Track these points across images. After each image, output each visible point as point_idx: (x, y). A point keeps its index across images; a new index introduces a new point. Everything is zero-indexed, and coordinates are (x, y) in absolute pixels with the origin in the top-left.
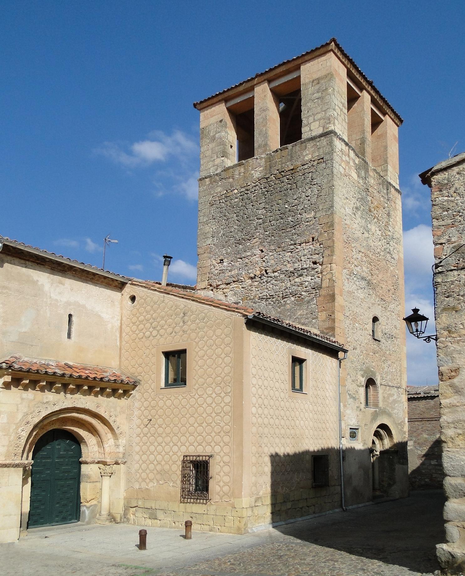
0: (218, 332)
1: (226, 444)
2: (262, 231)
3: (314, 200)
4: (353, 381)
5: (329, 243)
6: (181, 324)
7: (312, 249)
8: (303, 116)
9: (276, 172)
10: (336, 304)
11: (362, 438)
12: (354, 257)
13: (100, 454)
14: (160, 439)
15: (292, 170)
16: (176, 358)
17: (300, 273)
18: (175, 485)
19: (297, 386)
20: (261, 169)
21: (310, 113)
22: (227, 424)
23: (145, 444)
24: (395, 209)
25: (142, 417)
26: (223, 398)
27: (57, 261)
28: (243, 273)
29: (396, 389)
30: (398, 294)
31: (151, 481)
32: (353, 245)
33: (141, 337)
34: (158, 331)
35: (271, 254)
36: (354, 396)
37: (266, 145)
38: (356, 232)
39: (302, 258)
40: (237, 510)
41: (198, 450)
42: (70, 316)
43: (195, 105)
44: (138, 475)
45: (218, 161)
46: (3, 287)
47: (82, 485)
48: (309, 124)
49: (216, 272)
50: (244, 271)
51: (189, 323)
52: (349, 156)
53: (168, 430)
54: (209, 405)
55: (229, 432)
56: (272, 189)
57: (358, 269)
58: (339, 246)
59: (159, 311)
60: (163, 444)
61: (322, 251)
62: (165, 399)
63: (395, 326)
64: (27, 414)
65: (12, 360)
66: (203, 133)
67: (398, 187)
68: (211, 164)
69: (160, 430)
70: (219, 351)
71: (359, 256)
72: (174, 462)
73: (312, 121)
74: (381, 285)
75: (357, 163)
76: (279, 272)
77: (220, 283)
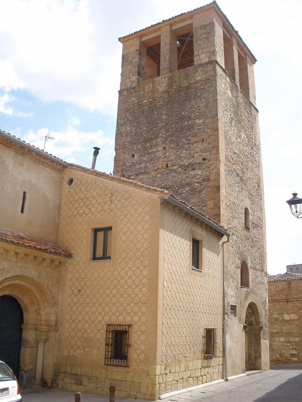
1: (143, 314)
6: (109, 203)
20: (165, 85)
22: (144, 295)
33: (75, 215)
42: (25, 193)
44: (68, 342)
47: (22, 349)
48: (199, 55)
49: (129, 164)
51: (116, 202)
54: (130, 277)
62: (93, 271)
70: (139, 227)
72: (98, 330)
77: (131, 174)
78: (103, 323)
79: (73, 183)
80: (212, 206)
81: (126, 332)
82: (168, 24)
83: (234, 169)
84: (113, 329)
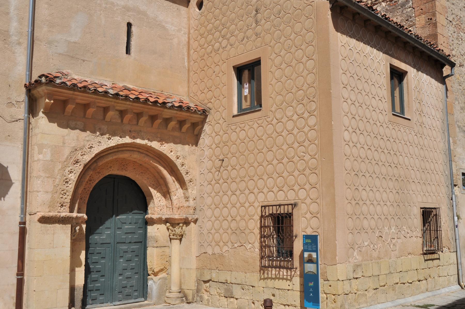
0: (298, 27)
6: (254, 25)
13: (168, 209)
16: (248, 71)
18: (253, 249)
19: (398, 109)
23: (217, 194)
26: (306, 120)
31: (225, 244)
33: (209, 51)
40: (330, 283)
41: (278, 198)
42: (129, 25)
51: (263, 21)
53: (242, 172)
55: (315, 168)
60: (238, 193)
64: (76, 150)
65: (55, 74)
69: (234, 174)
78: (256, 204)
79: (203, 6)
80: (423, 22)
81: (289, 216)
84: (271, 212)
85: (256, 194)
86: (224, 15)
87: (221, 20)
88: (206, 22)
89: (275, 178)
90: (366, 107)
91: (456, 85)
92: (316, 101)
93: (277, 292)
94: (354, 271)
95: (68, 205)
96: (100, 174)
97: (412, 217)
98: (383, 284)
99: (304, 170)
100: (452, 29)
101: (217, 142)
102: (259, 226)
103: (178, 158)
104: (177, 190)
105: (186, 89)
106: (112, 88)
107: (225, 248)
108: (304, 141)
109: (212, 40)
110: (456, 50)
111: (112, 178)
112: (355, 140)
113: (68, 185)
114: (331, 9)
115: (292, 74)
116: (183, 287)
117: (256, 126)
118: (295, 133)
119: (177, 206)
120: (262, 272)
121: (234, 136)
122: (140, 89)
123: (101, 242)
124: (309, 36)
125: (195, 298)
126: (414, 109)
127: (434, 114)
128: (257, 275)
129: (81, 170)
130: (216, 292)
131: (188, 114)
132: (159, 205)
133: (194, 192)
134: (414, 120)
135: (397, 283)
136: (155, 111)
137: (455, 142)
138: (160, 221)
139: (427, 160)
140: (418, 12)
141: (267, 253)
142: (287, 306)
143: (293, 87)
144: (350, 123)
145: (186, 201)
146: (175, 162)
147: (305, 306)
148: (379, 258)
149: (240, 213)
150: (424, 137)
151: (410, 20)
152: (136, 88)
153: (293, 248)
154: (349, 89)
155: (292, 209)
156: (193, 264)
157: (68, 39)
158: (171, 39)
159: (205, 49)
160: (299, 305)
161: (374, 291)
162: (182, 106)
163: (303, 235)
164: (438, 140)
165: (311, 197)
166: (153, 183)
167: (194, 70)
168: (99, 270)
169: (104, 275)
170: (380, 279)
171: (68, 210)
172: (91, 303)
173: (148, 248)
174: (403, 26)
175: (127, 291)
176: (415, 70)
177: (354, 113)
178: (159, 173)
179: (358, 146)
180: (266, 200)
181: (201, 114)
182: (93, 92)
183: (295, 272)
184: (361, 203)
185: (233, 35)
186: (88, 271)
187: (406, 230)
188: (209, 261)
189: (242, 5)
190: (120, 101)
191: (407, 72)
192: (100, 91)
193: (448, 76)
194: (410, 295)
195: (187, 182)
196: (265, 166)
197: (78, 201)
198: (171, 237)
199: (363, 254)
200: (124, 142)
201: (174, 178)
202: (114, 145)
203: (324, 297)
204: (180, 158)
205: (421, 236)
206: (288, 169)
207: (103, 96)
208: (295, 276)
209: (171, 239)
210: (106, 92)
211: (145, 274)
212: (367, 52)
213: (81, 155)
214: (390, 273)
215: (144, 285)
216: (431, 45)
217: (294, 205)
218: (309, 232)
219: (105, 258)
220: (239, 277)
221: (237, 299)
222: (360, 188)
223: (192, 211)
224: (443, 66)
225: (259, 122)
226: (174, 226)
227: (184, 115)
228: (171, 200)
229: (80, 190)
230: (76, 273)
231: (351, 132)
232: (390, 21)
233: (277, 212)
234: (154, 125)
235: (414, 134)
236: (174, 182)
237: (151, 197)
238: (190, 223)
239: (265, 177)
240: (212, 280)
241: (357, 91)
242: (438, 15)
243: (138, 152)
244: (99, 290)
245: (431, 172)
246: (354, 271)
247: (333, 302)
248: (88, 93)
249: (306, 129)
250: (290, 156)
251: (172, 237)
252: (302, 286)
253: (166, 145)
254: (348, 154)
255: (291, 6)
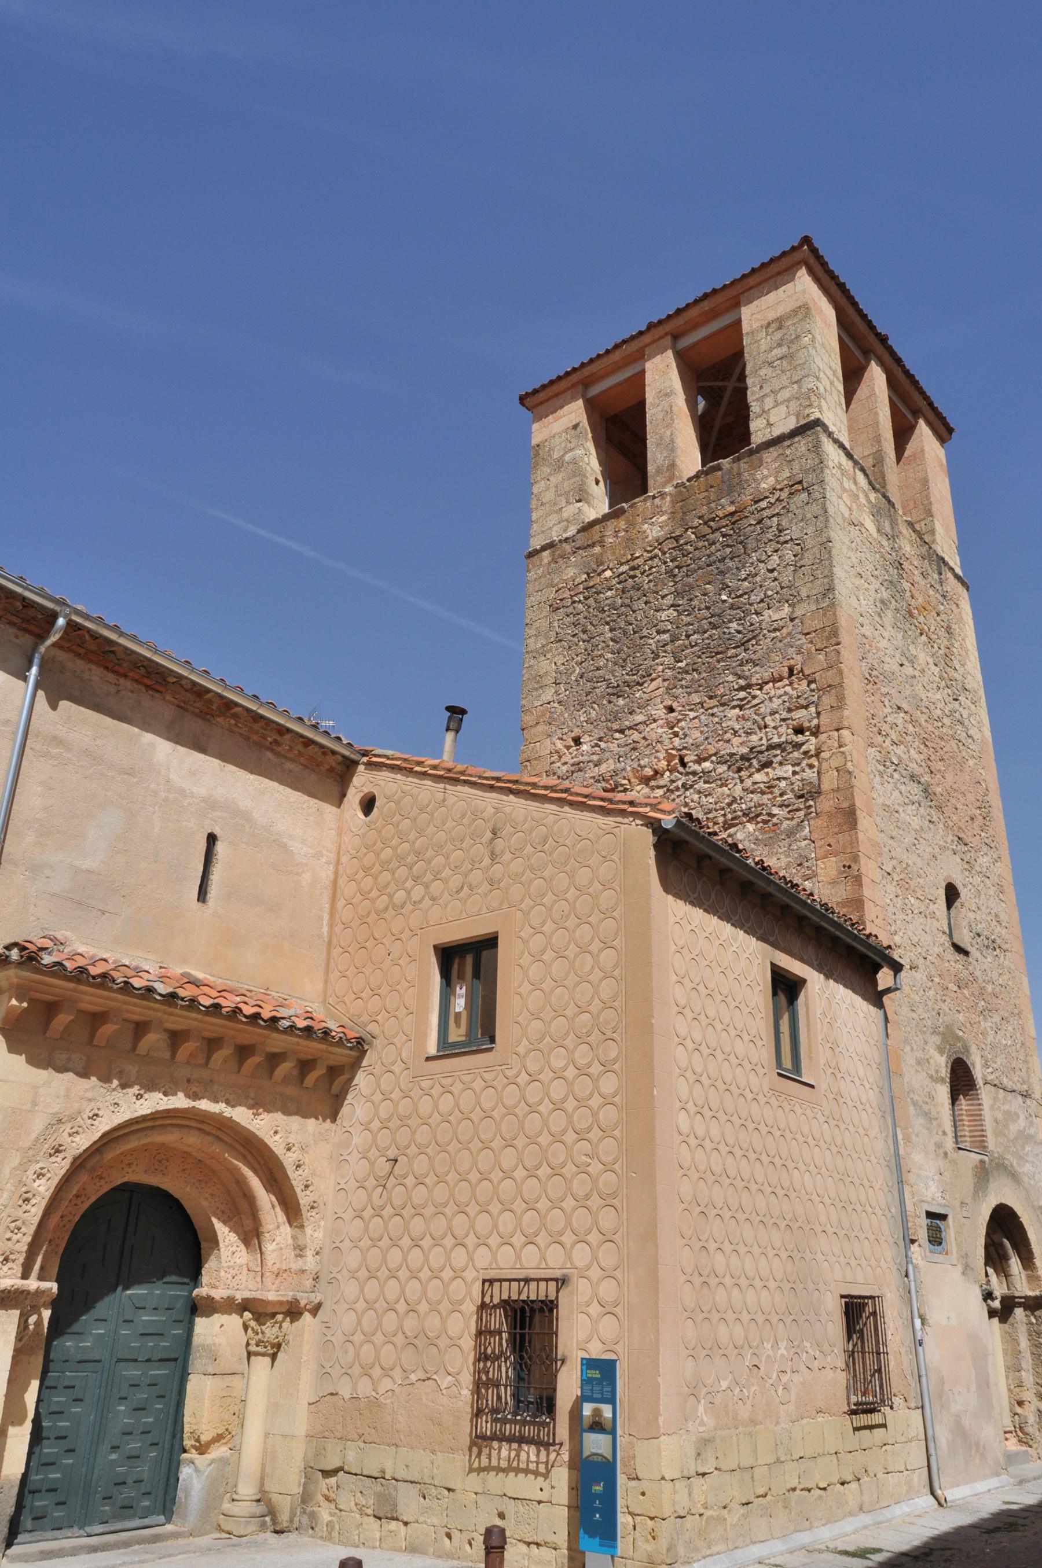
0: (583, 875)
2: (669, 660)
3: (787, 576)
4: (919, 1063)
5: (830, 677)
6: (487, 861)
7: (791, 697)
8: (751, 397)
9: (696, 522)
10: (861, 835)
11: (959, 1247)
12: (889, 719)
14: (418, 1225)
15: (732, 514)
16: (469, 961)
17: (763, 758)
18: (454, 1389)
19: (787, 1063)
20: (664, 518)
21: (767, 389)
22: (608, 1168)
24: (960, 620)
25: (373, 1153)
26: (595, 1080)
27: (194, 684)
28: (629, 769)
29: (1020, 1098)
30: (991, 832)
31: (387, 1372)
32: (884, 690)
33: (382, 907)
34: (427, 886)
35: (692, 714)
36: (926, 1108)
37: (673, 466)
38: (887, 659)
39: (768, 719)
40: (644, 1485)
41: (524, 1259)
42: (212, 839)
43: (522, 399)
44: (351, 1350)
45: (569, 511)
46: (54, 738)
49: (565, 768)
50: (629, 762)
51: (507, 856)
52: (855, 483)
53: (441, 1193)
55: (614, 1195)
56: (689, 562)
57: (900, 750)
58: (853, 685)
59: (432, 829)
61: (815, 699)
62: (436, 1091)
63: (996, 916)
64: (60, 1121)
65: (42, 943)
66: (537, 455)
67: (959, 571)
68: (553, 519)
69: (420, 1194)
71: (900, 718)
73: (771, 405)
74: (953, 801)
75: (873, 501)
76: (714, 758)
78: (470, 1274)
79: (375, 809)
80: (834, 872)
81: (549, 1307)
82: (666, 334)
83: (899, 758)
84: (505, 1297)
85: (471, 1248)
86: (421, 833)
87: (414, 843)
88: (379, 842)
89: (519, 1212)
90: (724, 1056)
91: (905, 1011)
92: (618, 1039)
93: (510, 1508)
94: (699, 1454)
95: (22, 1260)
96: (103, 1182)
97: (824, 1318)
98: (761, 1491)
99: (587, 1197)
100: (891, 888)
101: (383, 1115)
102: (473, 1331)
103: (289, 1149)
104: (278, 1227)
105: (320, 987)
106: (162, 979)
107: (386, 1384)
108: (589, 1129)
109: (388, 884)
110: (901, 934)
111: (129, 1191)
112: (700, 1132)
113: (29, 1207)
114: (656, 846)
115: (567, 975)
116: (270, 1486)
117: (478, 1084)
118: (570, 1110)
119: (275, 1269)
120: (475, 1450)
121: (425, 1105)
122: (220, 983)
123: (79, 1357)
124: (607, 898)
125: (296, 1519)
126: (822, 1062)
127: (861, 1074)
128: (461, 1460)
129: (63, 1171)
130: (353, 1503)
131: (324, 1047)
132: (232, 1264)
133: (319, 1235)
134: (822, 1086)
135: (794, 1489)
136: (249, 1035)
137: (907, 1139)
138: (231, 1306)
139: (850, 1179)
140: (823, 850)
141: (490, 1402)
142: (534, 1547)
143: (567, 1005)
144: (691, 1093)
145: (297, 1256)
146: (281, 1158)
147: (582, 1548)
148: (753, 1422)
149: (430, 1295)
150: (843, 1127)
151: (806, 864)
152: (211, 979)
153: (555, 1390)
154: (690, 1015)
155: (557, 1292)
156: (301, 1423)
157: (77, 863)
158: (297, 874)
159: (373, 901)
160: (566, 1545)
161: (743, 1510)
162: (312, 1027)
163: (582, 1359)
164: (873, 1133)
165: (603, 1264)
166: (222, 1207)
167: (342, 944)
168: (63, 1434)
169: (73, 1447)
170: (756, 1478)
171: (18, 1270)
172: (30, 1527)
173: (190, 1376)
174: (797, 885)
175: (128, 1493)
176: (822, 976)
177: (699, 1070)
178: (241, 1183)
179: (708, 1145)
180: (494, 1266)
181: (351, 1049)
182: (121, 988)
183: (558, 1454)
184: (713, 1282)
185: (438, 877)
186: (37, 1437)
187: (810, 1351)
188: (344, 1416)
189: (463, 816)
190: (178, 1011)
191: (804, 981)
192: (137, 986)
193: (888, 991)
194: (823, 1522)
195: (304, 1210)
196: (495, 1181)
197: (44, 1248)
198: (251, 1348)
199: (705, 1403)
200: (171, 1107)
201: (273, 1198)
202: (149, 1112)
203: (628, 1524)
204: (294, 1149)
205: (844, 1367)
206: (549, 1192)
207: (142, 997)
208: (556, 1464)
209: (249, 1354)
210: (150, 990)
211: (177, 1447)
212: (725, 937)
213: (70, 1135)
214: (778, 1461)
215: (168, 1479)
216: (853, 925)
217: (562, 1282)
218: (596, 1351)
219: (82, 1400)
220: (414, 1461)
221: (406, 1524)
222: (712, 1246)
223: (308, 1283)
224: (877, 968)
225: (486, 1076)
226: (262, 1320)
227: (313, 1047)
228: (261, 1253)
229: (54, 1220)
230: (9, 1441)
231: (692, 1113)
232: (772, 874)
233: (520, 1293)
234: (243, 1069)
235: (822, 1119)
236: (273, 1206)
237: (215, 1242)
238: (301, 1314)
239: (495, 1208)
240: (346, 1468)
241: (705, 1022)
242: (863, 860)
243: (200, 1129)
244: (55, 1490)
245: (859, 1209)
246: (699, 1454)
247: (650, 1537)
248: (110, 989)
249: (595, 1102)
250: (554, 1162)
251: (253, 1348)
252: (574, 1492)
253: (265, 1116)
254: (686, 1165)
255: (570, 830)
